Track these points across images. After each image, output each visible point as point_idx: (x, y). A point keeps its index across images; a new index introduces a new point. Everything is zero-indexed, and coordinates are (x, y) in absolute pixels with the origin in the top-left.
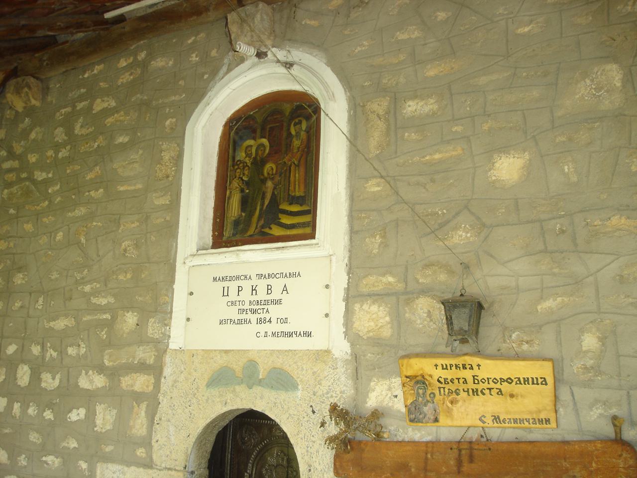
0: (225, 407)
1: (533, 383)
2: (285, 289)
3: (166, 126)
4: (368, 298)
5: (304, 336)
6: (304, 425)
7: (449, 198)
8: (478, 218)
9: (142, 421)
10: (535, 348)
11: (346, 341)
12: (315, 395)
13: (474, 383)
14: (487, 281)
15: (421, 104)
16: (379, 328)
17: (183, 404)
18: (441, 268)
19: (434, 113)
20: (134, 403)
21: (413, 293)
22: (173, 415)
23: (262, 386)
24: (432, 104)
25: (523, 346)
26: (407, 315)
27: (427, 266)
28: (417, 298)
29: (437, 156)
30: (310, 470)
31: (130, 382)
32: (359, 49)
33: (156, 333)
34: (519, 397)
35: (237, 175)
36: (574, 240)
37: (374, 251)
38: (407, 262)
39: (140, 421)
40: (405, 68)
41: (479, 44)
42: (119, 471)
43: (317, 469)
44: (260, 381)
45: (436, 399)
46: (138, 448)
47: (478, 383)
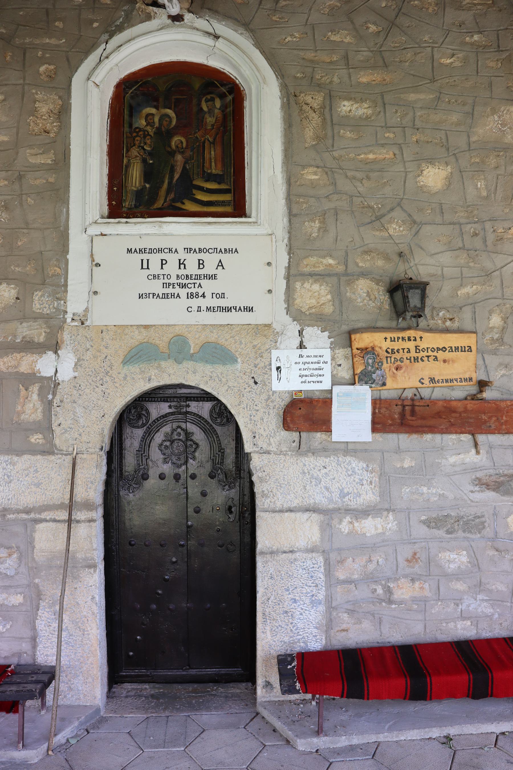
0: (149, 383)
1: (462, 351)
2: (220, 264)
3: (40, 72)
4: (310, 277)
5: (244, 311)
6: (245, 395)
7: (383, 195)
8: (410, 215)
9: (34, 405)
10: (456, 325)
11: (288, 316)
12: (256, 367)
13: (416, 352)
14: (422, 267)
15: (355, 106)
16: (321, 305)
17: (92, 383)
18: (378, 254)
19: (367, 118)
20: (21, 385)
21: (353, 275)
22: (80, 395)
23: (193, 361)
24: (365, 108)
25: (447, 323)
26: (348, 294)
27: (366, 252)
28: (357, 280)
29: (371, 156)
30: (255, 437)
31: (13, 363)
32: (289, 39)
33: (45, 307)
34: (451, 362)
35: (137, 143)
36: (485, 241)
37: (313, 235)
38: (347, 247)
39: (32, 405)
40: (339, 69)
41: (407, 64)
42: (6, 462)
43: (262, 435)
44: (192, 355)
45: (383, 367)
46: (33, 435)
47: (419, 352)
